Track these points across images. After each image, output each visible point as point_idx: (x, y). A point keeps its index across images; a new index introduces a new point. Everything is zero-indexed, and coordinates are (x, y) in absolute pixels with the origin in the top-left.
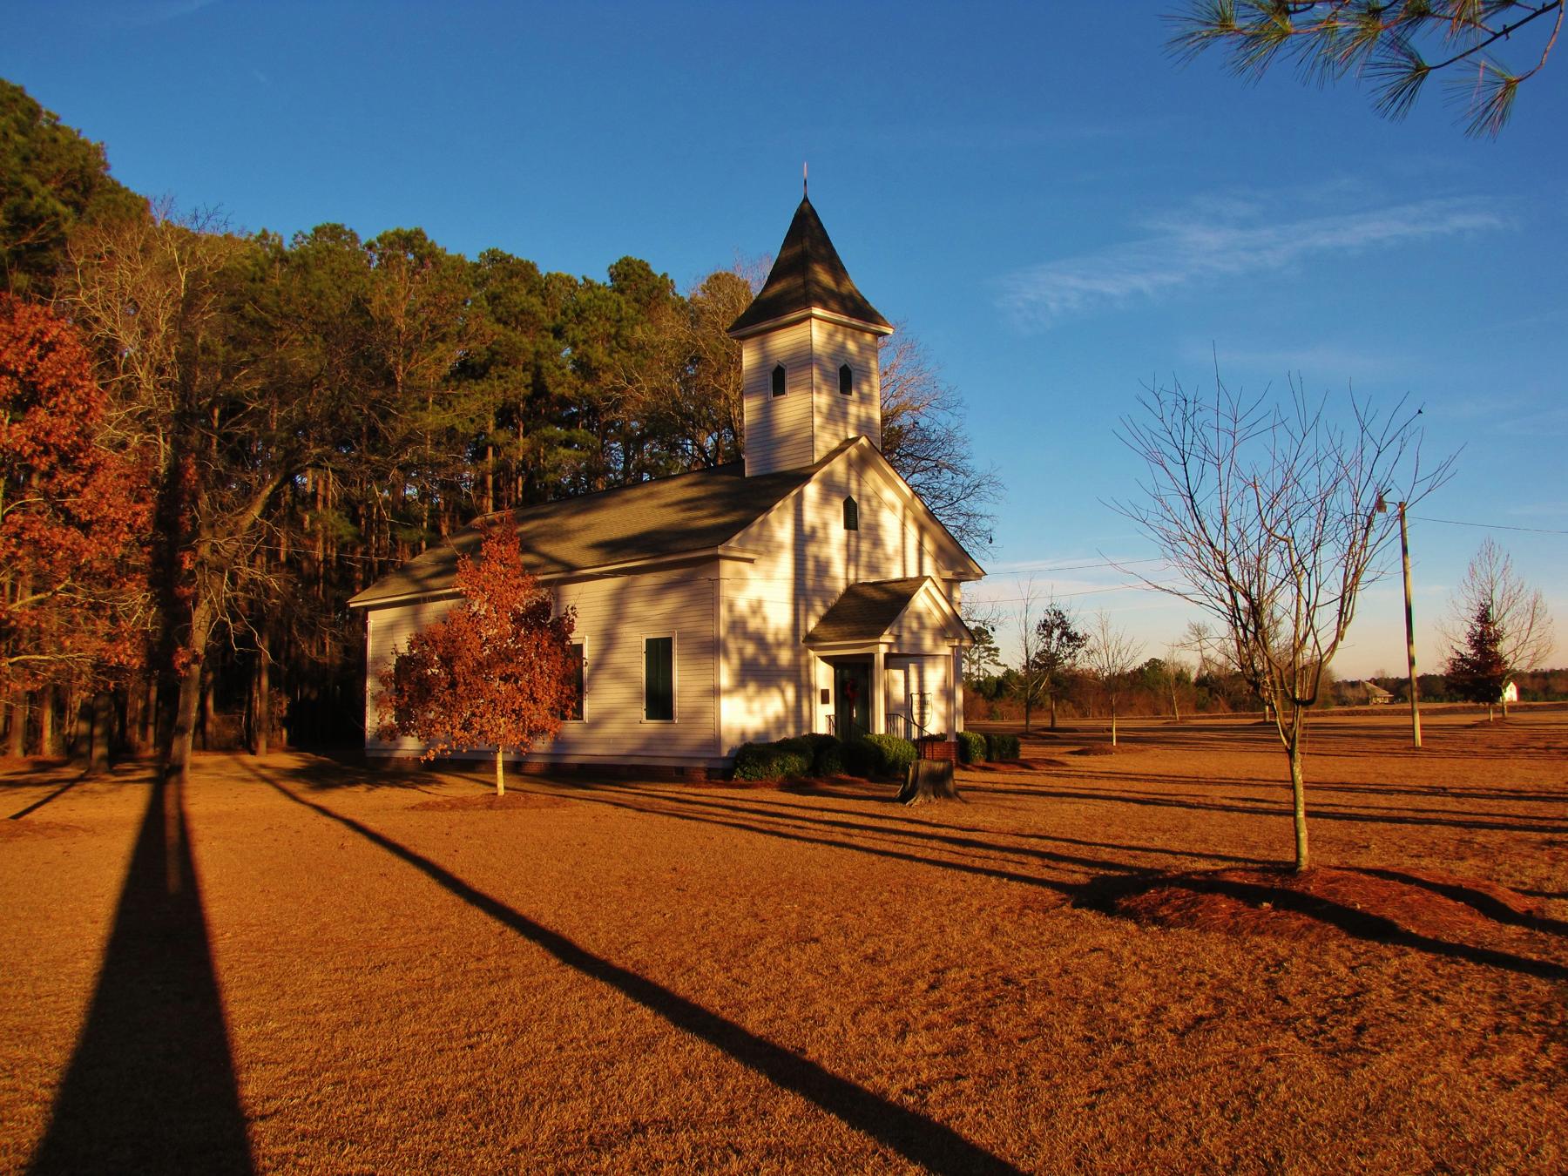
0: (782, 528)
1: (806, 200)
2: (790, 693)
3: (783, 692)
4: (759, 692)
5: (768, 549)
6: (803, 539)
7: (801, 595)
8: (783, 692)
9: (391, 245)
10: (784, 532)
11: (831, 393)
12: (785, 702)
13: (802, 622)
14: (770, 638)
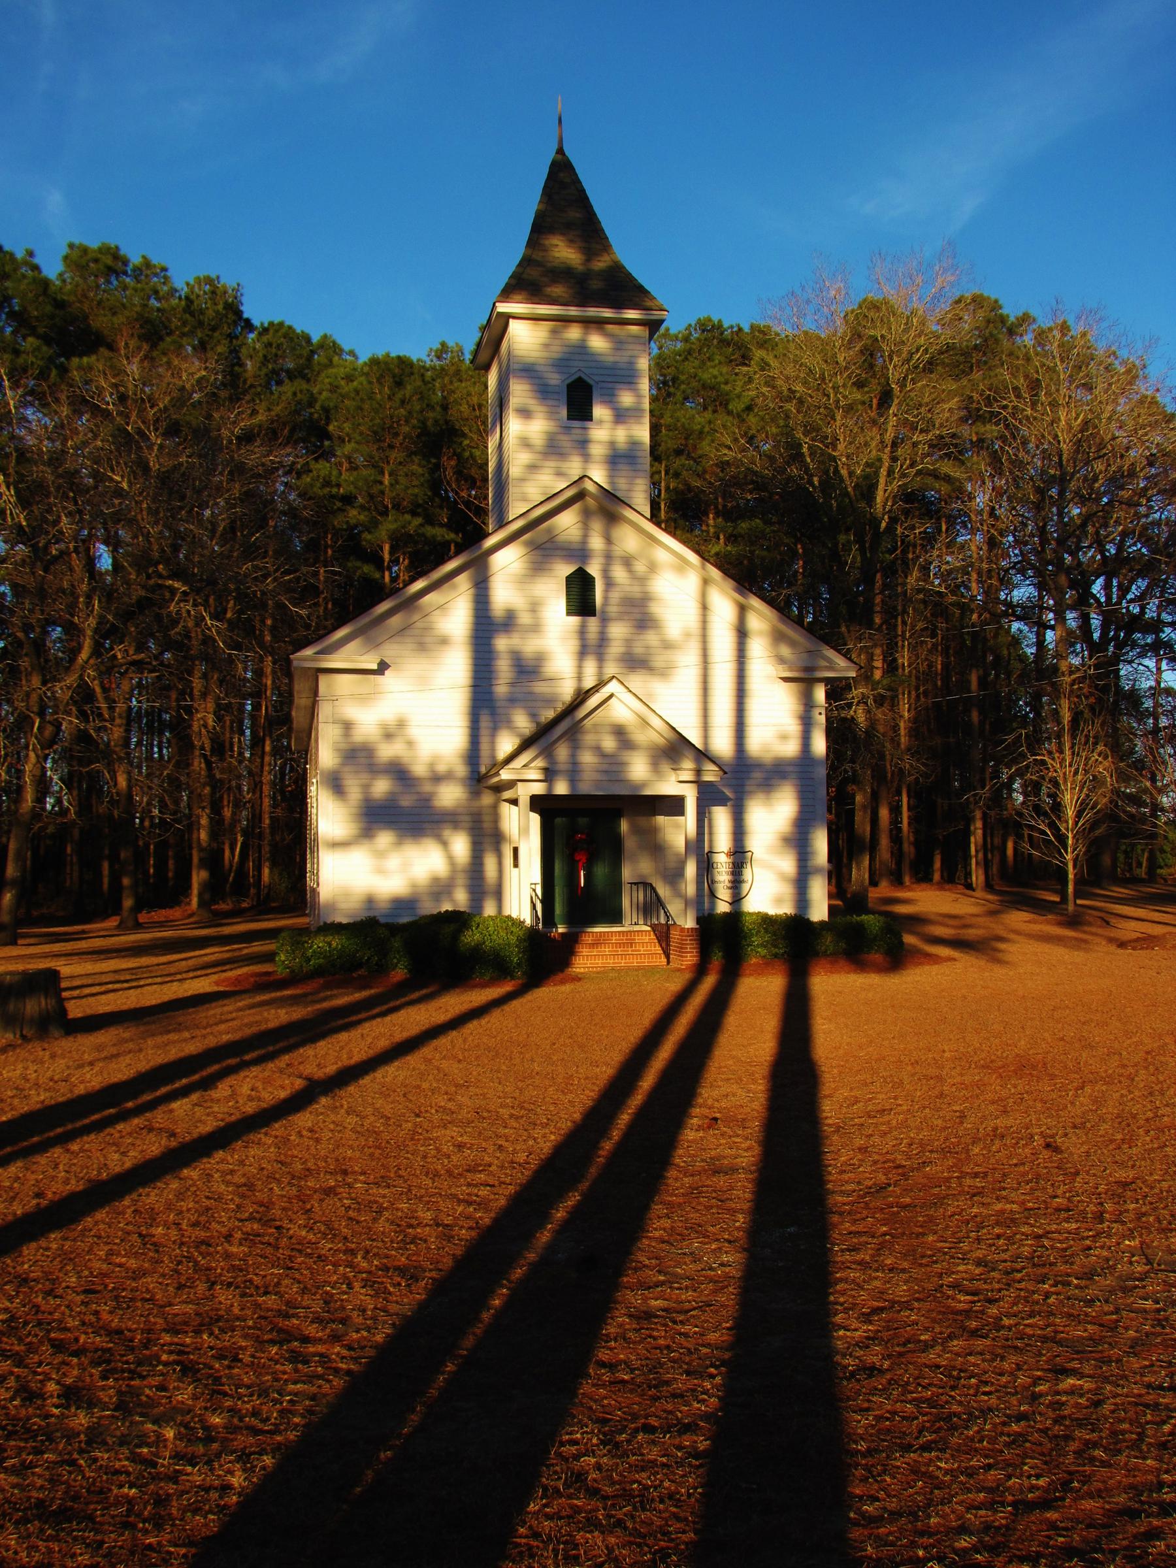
0: (453, 613)
1: (560, 151)
2: (460, 845)
3: (445, 844)
4: (399, 843)
5: (428, 644)
6: (486, 627)
7: (483, 705)
8: (445, 844)
9: (1065, 349)
10: (453, 613)
11: (551, 415)
12: (451, 859)
13: (484, 747)
14: (419, 769)
